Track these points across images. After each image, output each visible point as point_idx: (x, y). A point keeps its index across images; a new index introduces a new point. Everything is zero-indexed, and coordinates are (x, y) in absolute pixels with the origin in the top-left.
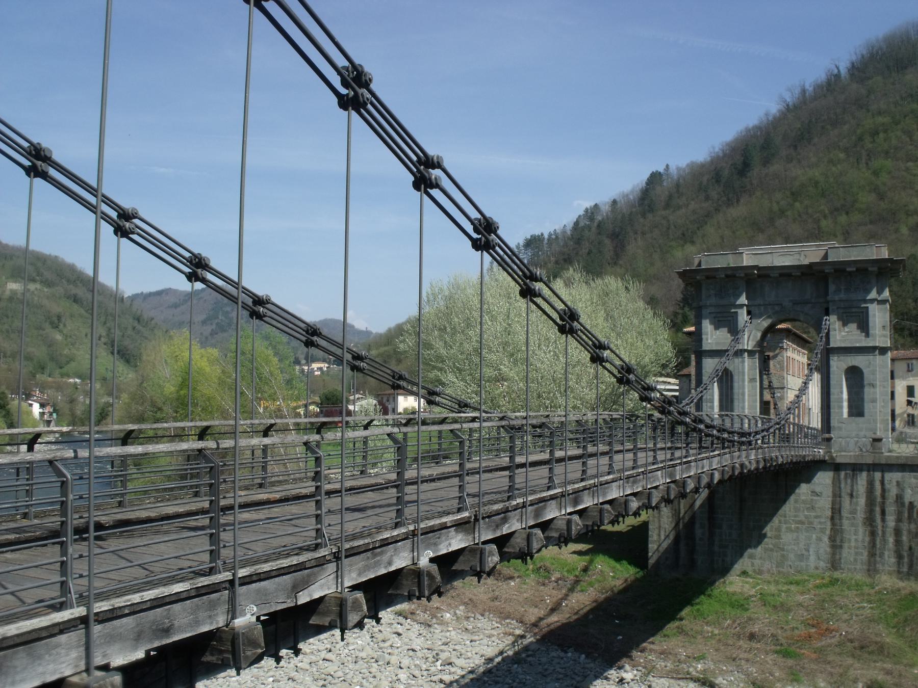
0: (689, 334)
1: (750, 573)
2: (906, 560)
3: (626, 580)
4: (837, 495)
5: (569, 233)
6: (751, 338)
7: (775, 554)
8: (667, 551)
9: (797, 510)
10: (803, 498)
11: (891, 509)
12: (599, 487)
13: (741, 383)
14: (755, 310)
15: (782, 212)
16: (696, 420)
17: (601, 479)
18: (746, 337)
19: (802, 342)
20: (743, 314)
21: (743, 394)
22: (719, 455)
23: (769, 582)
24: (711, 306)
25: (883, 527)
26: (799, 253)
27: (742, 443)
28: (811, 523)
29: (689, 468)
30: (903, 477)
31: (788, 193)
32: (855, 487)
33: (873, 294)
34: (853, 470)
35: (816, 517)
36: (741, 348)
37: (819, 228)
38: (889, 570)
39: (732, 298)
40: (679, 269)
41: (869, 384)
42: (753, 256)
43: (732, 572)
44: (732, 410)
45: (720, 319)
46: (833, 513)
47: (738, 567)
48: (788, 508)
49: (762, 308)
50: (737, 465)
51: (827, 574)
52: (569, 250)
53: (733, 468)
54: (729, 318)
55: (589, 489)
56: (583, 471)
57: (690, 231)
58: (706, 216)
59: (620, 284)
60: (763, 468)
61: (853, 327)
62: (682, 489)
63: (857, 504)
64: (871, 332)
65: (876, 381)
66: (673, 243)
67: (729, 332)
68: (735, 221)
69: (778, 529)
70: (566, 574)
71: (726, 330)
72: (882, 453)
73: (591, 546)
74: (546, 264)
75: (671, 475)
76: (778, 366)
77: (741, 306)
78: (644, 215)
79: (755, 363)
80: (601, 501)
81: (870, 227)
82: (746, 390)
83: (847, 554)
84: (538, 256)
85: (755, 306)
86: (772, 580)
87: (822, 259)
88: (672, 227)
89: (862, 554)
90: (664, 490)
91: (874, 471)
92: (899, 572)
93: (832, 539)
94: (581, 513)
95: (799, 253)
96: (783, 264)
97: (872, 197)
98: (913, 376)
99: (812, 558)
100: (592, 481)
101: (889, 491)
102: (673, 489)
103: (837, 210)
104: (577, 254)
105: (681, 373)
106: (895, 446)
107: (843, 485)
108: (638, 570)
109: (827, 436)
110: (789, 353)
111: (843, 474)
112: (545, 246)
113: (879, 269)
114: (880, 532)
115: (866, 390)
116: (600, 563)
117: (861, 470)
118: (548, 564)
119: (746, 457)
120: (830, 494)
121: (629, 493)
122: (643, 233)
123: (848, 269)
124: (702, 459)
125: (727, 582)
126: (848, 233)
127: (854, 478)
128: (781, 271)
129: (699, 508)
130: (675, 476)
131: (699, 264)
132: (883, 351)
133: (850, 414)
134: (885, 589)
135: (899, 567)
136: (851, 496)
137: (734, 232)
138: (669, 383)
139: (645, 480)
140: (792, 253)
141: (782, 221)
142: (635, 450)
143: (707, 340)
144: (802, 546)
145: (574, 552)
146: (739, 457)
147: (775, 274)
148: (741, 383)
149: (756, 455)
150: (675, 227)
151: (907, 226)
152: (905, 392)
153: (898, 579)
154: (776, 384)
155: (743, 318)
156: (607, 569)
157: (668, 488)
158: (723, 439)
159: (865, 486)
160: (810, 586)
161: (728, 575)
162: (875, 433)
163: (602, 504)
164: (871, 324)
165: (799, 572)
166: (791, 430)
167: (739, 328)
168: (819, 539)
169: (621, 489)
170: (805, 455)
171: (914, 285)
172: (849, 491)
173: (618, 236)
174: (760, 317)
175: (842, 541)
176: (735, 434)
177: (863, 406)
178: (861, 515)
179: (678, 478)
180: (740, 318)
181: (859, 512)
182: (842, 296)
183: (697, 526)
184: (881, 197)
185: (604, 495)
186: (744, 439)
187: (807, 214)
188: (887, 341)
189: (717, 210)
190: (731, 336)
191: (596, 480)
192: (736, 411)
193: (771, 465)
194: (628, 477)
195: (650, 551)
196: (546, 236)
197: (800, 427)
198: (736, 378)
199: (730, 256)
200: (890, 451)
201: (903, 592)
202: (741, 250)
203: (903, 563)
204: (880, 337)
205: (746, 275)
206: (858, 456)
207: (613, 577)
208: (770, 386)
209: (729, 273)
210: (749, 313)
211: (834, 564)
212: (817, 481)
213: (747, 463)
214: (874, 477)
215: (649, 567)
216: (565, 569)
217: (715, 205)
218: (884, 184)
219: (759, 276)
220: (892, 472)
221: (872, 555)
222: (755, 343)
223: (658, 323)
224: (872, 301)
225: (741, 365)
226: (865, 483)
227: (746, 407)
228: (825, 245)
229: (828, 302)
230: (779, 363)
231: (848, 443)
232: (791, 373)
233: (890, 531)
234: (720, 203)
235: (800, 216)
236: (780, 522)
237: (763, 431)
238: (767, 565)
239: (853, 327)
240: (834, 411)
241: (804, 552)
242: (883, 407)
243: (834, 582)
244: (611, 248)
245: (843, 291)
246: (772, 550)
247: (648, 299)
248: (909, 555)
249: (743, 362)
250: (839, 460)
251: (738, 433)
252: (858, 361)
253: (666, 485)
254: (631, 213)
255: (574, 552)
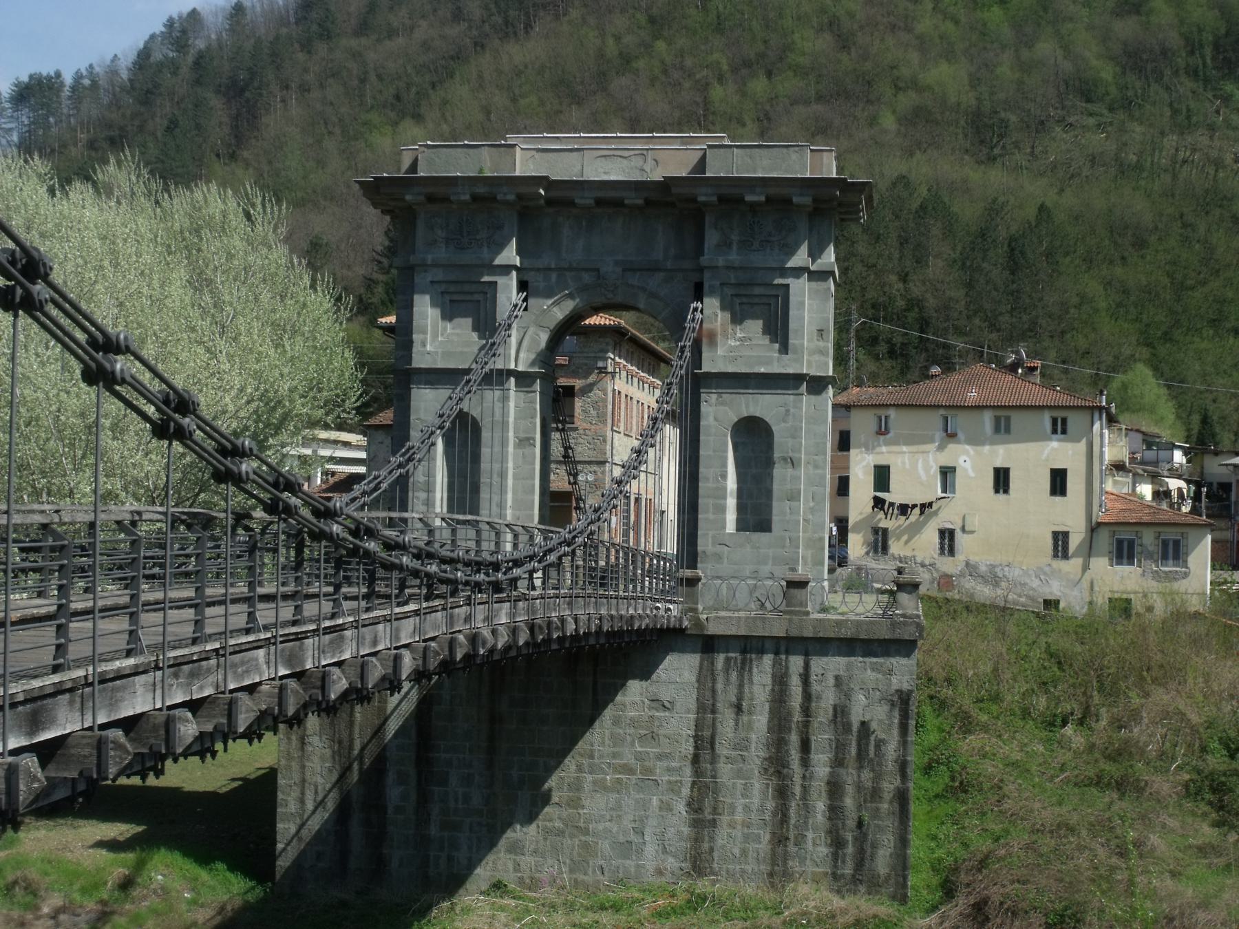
0: (389, 329)
1: (512, 886)
2: (850, 849)
3: (222, 909)
4: (706, 708)
5: (125, 75)
6: (525, 343)
7: (568, 842)
8: (318, 837)
9: (617, 740)
10: (632, 714)
11: (822, 738)
12: (97, 687)
13: (497, 449)
14: (531, 277)
15: (626, 60)
16: (358, 528)
17: (103, 667)
18: (514, 341)
19: (650, 359)
20: (508, 287)
21: (503, 475)
22: (416, 613)
23: (553, 907)
24: (435, 265)
25: (804, 777)
26: (643, 154)
27: (477, 587)
28: (648, 771)
29: (338, 645)
30: (849, 667)
31: (642, 18)
32: (746, 690)
33: (800, 258)
34: (744, 651)
35: (660, 757)
36: (499, 366)
37: (706, 102)
38: (813, 873)
39: (485, 250)
40: (365, 174)
41: (784, 459)
42: (537, 155)
43: (471, 885)
44: (475, 510)
45: (456, 297)
46: (696, 748)
47: (483, 874)
48: (598, 737)
49: (554, 276)
50: (461, 637)
51: (684, 884)
52: (123, 115)
53: (452, 644)
54: (476, 297)
55: (71, 690)
56: (58, 647)
57: (414, 90)
58: (452, 58)
59: (232, 204)
60: (527, 644)
61: (754, 327)
62: (319, 692)
63: (749, 727)
64: (792, 341)
65: (800, 452)
66: (374, 117)
67: (476, 328)
68: (519, 74)
69: (577, 786)
70: (77, 896)
71: (468, 322)
72: (807, 613)
73: (140, 829)
74: (64, 146)
75: (290, 660)
76: (593, 413)
77: (506, 269)
78: (307, 46)
79: (533, 402)
80: (101, 720)
81: (818, 108)
82: (510, 465)
83: (727, 839)
84: (47, 127)
85: (538, 270)
86: (559, 901)
87: (693, 171)
88: (373, 77)
89: (758, 839)
90: (270, 695)
91: (788, 653)
92: (835, 876)
93: (695, 806)
94: (47, 752)
95: (643, 154)
96: (605, 178)
97: (824, 43)
98: (887, 444)
99: (650, 849)
100: (80, 673)
101: (819, 698)
102: (296, 692)
103: (747, 64)
104: (141, 128)
105: (372, 421)
106: (835, 600)
107: (720, 686)
108: (253, 883)
109: (688, 573)
110: (620, 384)
111: (720, 659)
112: (66, 103)
113: (815, 200)
114: (797, 790)
115: (778, 471)
116: (161, 868)
117: (761, 652)
118: (33, 874)
119: (486, 619)
120: (693, 706)
121: (179, 699)
122: (304, 89)
123: (748, 198)
124: (375, 622)
125: (458, 909)
126: (769, 119)
127: (745, 667)
128: (601, 194)
129: (396, 735)
130: (302, 661)
131: (414, 167)
132: (817, 385)
133: (742, 526)
134: (804, 914)
135: (835, 866)
136: (738, 708)
137: (514, 100)
138: (347, 444)
139: (221, 671)
140: (626, 154)
141: (624, 81)
142: (199, 605)
143: (424, 345)
144: (627, 823)
145: (100, 844)
146: (468, 619)
147: (585, 199)
148: (497, 449)
149: (512, 615)
150: (380, 77)
151: (894, 112)
152: (871, 479)
153: (831, 890)
154: (582, 451)
155: (509, 299)
156: (176, 884)
157: (282, 689)
158: (428, 575)
159: (769, 688)
160: (645, 912)
161: (461, 891)
162: (794, 570)
163: (103, 727)
164: (792, 325)
165: (620, 882)
166: (613, 559)
167: (499, 319)
168: (666, 807)
169: (159, 692)
170: (632, 617)
171: (901, 244)
172: (734, 699)
173: (242, 91)
174: (549, 296)
175: (715, 811)
176: (460, 566)
177: (770, 507)
178: (757, 753)
179: (309, 665)
180: (501, 298)
181: (753, 745)
182: (734, 257)
183: (391, 777)
184: (844, 43)
185: (113, 705)
186: (481, 577)
187: (682, 68)
188: (827, 364)
189: (479, 45)
190: (480, 338)
191: (91, 669)
192: (482, 512)
193: (548, 641)
194: (177, 664)
195: (278, 838)
196: (68, 79)
197: (633, 554)
198: (485, 435)
199: (485, 151)
200: (824, 610)
201: (841, 920)
202: (512, 138)
203: (845, 855)
204: (811, 353)
205: (520, 197)
206: (754, 619)
207: (194, 902)
208: (566, 456)
209: (481, 190)
210: (523, 286)
211: (698, 864)
212: (663, 676)
213: (486, 633)
214: (787, 668)
215: (278, 877)
216: (76, 887)
217: (475, 32)
218: (851, 15)
219: (550, 202)
220: (826, 655)
221: (779, 840)
222: (533, 356)
223: (321, 302)
224: (798, 272)
225: (498, 405)
226: (768, 680)
227: (509, 503)
228: (702, 140)
229: (701, 270)
230: (595, 405)
231: (733, 591)
232: (622, 429)
233: (819, 786)
234: (487, 27)
235: (665, 72)
236: (580, 769)
237: (531, 558)
238: (549, 868)
239: (754, 327)
240: (705, 516)
241: (633, 837)
242: (812, 510)
243: (696, 902)
244: (225, 119)
245: (735, 247)
246: (561, 833)
247: (305, 246)
248: (855, 839)
249: (505, 399)
250: (713, 629)
251: (467, 564)
252: (763, 405)
253: (277, 683)
254: (277, 38)
255: (100, 844)
